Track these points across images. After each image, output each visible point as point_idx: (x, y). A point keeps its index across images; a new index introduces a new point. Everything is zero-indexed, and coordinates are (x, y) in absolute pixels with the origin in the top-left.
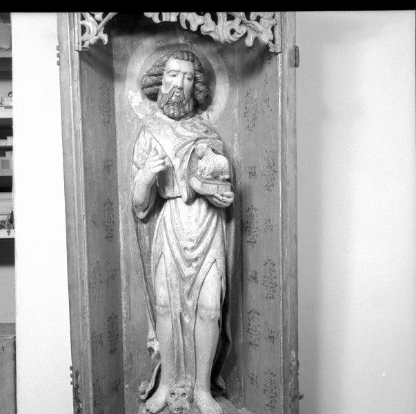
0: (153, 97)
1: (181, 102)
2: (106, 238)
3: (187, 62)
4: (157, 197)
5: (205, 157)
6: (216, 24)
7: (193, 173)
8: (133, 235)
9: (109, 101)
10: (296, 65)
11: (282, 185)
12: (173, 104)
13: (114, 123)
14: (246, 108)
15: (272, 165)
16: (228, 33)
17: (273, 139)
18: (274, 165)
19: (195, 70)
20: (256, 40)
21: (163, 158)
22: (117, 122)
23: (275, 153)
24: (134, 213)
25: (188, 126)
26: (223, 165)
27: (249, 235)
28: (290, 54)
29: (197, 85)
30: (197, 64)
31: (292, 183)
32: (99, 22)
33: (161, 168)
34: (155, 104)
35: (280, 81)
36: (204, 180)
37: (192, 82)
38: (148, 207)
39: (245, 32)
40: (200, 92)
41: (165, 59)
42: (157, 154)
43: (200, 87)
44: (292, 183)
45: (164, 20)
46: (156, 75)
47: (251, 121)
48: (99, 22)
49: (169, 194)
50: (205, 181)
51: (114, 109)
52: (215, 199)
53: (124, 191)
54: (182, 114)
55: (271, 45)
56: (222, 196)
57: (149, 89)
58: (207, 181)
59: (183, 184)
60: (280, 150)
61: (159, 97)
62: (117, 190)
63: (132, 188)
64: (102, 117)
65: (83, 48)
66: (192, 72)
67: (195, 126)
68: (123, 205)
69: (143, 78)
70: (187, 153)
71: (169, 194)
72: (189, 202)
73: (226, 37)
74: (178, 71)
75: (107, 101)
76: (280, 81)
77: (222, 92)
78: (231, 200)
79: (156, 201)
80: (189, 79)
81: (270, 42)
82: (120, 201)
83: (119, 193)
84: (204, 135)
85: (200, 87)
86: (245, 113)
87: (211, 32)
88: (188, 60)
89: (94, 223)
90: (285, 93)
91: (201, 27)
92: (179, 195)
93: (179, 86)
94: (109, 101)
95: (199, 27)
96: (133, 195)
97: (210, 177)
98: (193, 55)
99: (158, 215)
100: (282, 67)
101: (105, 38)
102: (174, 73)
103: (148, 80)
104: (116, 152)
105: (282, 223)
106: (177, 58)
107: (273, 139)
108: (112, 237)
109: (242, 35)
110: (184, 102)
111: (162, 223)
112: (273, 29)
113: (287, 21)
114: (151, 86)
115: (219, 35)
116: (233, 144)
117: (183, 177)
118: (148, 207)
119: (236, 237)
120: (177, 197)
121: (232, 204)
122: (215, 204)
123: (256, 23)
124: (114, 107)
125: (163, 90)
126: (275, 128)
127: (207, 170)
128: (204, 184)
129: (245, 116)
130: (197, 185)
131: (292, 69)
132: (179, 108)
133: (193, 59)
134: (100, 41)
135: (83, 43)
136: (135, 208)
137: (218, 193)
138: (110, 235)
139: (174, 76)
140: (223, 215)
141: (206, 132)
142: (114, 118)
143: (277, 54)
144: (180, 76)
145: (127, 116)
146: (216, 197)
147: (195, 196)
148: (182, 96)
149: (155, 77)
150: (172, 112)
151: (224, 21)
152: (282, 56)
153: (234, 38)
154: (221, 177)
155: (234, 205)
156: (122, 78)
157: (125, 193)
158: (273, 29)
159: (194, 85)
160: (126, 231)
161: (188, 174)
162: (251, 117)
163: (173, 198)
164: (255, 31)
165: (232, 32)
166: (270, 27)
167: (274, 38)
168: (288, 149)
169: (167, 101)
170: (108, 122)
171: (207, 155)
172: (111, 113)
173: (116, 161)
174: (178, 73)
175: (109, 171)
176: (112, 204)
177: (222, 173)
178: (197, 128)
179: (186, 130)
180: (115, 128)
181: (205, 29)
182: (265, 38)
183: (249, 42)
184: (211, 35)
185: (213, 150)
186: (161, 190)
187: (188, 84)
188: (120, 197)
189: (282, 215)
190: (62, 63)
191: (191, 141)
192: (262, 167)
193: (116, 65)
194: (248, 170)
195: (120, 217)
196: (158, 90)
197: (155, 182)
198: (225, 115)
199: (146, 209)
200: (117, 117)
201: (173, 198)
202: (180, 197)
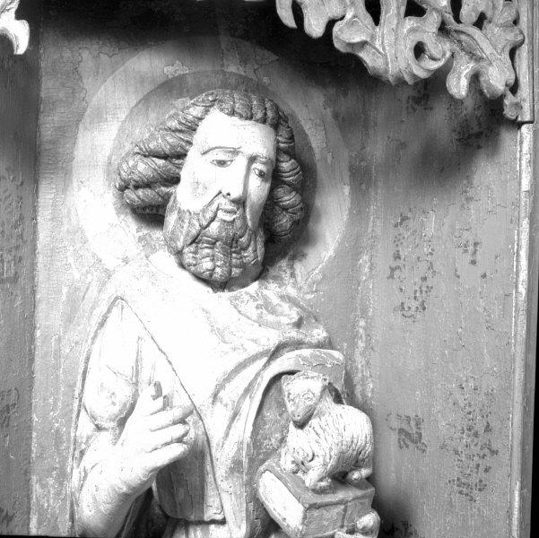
0: (152, 215)
5: (314, 422)
6: (377, 21)
7: (268, 455)
9: (21, 218)
12: (213, 244)
15: (480, 427)
16: (410, 54)
17: (487, 357)
18: (488, 429)
20: (475, 78)
22: (41, 276)
25: (251, 309)
26: (361, 442)
30: (284, 133)
37: (268, 185)
41: (196, 111)
42: (167, 404)
43: (288, 198)
46: (165, 157)
51: (34, 240)
53: (49, 472)
57: (140, 192)
61: (171, 219)
62: (27, 473)
63: (69, 471)
66: (272, 155)
67: (267, 306)
70: (247, 391)
73: (402, 65)
74: (235, 152)
80: (261, 174)
83: (34, 478)
84: (294, 334)
85: (288, 198)
86: (393, 270)
87: (363, 44)
91: (336, 29)
92: (219, 517)
94: (21, 218)
95: (331, 24)
96: (74, 504)
102: (222, 157)
103: (142, 167)
104: (32, 360)
106: (233, 113)
107: (487, 357)
110: (243, 240)
114: (148, 185)
117: (236, 466)
124: (35, 232)
127: (317, 463)
129: (391, 277)
132: (227, 254)
133: (278, 121)
139: (222, 163)
141: (298, 325)
142: (33, 266)
144: (241, 162)
145: (71, 260)
148: (238, 223)
149: (161, 162)
150: (206, 265)
156: (63, 168)
157: (51, 481)
161: (251, 460)
164: (472, 55)
165: (419, 50)
167: (517, 81)
169: (194, 232)
171: (321, 414)
172: (25, 251)
173: (31, 387)
174: (227, 153)
178: (273, 312)
179: (255, 318)
180: (34, 292)
184: (364, 55)
187: (257, 189)
188: (37, 489)
191: (262, 354)
193: (49, 124)
197: (150, 480)
200: (41, 259)
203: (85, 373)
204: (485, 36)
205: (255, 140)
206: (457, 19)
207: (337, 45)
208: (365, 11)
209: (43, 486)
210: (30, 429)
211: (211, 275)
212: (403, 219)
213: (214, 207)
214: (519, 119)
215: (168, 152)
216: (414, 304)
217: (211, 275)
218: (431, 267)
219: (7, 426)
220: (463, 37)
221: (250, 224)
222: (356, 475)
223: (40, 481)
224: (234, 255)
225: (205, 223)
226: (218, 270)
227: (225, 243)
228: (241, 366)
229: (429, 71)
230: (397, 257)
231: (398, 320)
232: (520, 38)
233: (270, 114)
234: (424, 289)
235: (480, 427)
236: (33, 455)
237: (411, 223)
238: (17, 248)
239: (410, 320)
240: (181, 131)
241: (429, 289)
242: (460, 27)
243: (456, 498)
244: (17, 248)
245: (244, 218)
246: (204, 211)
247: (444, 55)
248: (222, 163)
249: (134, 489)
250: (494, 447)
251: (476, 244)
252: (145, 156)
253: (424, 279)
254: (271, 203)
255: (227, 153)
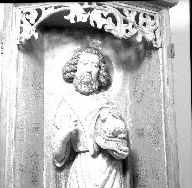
0: (70, 80)
1: (90, 82)
2: (32, 182)
3: (95, 55)
4: (71, 151)
6: (116, 25)
8: (52, 181)
10: (172, 57)
11: (166, 142)
13: (43, 98)
14: (135, 89)
15: (156, 127)
16: (125, 32)
18: (158, 127)
19: (100, 61)
20: (144, 38)
21: (76, 121)
23: (159, 119)
24: (54, 163)
26: (121, 127)
27: (140, 181)
28: (167, 48)
29: (101, 72)
31: (173, 141)
32: (32, 25)
33: (72, 129)
34: (71, 86)
35: (161, 67)
36: (107, 138)
37: (98, 68)
38: (64, 158)
39: (136, 32)
40: (104, 77)
44: (173, 141)
45: (78, 21)
46: (73, 65)
47: (139, 97)
48: (32, 25)
49: (80, 148)
50: (109, 139)
51: (44, 89)
52: (115, 153)
54: (91, 91)
55: (154, 42)
56: (120, 150)
58: (109, 139)
59: (91, 140)
60: (163, 116)
61: (75, 80)
62: (43, 145)
64: (34, 93)
65: (20, 42)
66: (99, 63)
68: (47, 156)
69: (64, 67)
71: (80, 148)
72: (95, 156)
73: (123, 34)
75: (39, 82)
76: (161, 67)
77: (118, 76)
78: (127, 154)
79: (71, 154)
80: (96, 67)
81: (153, 40)
82: (44, 153)
83: (44, 147)
86: (135, 92)
87: (111, 30)
88: (95, 54)
89: (22, 170)
90: (166, 75)
91: (105, 27)
92: (87, 150)
93: (89, 71)
94: (40, 83)
95: (104, 26)
97: (111, 135)
98: (99, 51)
99: (72, 164)
100: (163, 57)
101: (36, 35)
104: (43, 118)
105: (168, 173)
106: (87, 52)
108: (36, 181)
109: (134, 34)
110: (92, 82)
111: (74, 171)
112: (154, 32)
113: (165, 27)
115: (118, 32)
116: (126, 113)
117: (91, 136)
118: (64, 158)
119: (130, 182)
120: (86, 151)
121: (127, 158)
122: (115, 157)
123: (143, 27)
125: (78, 74)
126: (158, 101)
128: (106, 141)
129: (134, 94)
130: (103, 144)
131: (170, 59)
134: (33, 37)
135: (21, 38)
136: (56, 158)
137: (117, 148)
138: (35, 180)
139: (85, 64)
140: (121, 165)
141: (108, 104)
143: (158, 48)
146: (115, 152)
147: (101, 151)
148: (90, 78)
149: (72, 66)
151: (121, 23)
152: (162, 50)
153: (128, 35)
154: (119, 136)
155: (129, 157)
157: (49, 148)
158: (154, 32)
159: (99, 72)
160: (48, 177)
161: (94, 134)
162: (138, 95)
163: (84, 152)
164: (143, 32)
165: (127, 31)
166: (153, 31)
168: (169, 116)
169: (80, 81)
170: (39, 97)
172: (41, 91)
175: (37, 131)
176: (38, 156)
177: (120, 133)
180: (44, 101)
181: (107, 28)
182: (150, 37)
183: (139, 39)
184: (112, 32)
185: (114, 116)
186: (74, 146)
187: (95, 71)
188: (45, 150)
189: (167, 166)
190: (4, 53)
192: (148, 129)
194: (138, 132)
195: (44, 165)
196: (74, 75)
198: (121, 94)
199: (63, 160)
201: (84, 152)
202: (88, 151)
203: (66, 152)
204: (147, 28)
205: (95, 59)
206: (138, 24)
207: (106, 30)
208: (112, 23)
209: (47, 149)
210: (43, 134)
211: (84, 91)
212: (136, 79)
213: (84, 75)
214: (158, 47)
215: (73, 63)
216: (140, 99)
217: (84, 91)
218: (143, 89)
219: (37, 132)
220: (139, 28)
221: (94, 79)
222: (119, 136)
223: (46, 148)
224: (90, 87)
225: (82, 79)
226: (86, 90)
227: (87, 83)
228: (92, 112)
229: (131, 36)
230: (135, 89)
231: (137, 105)
232: (156, 28)
233: (97, 52)
234: (142, 95)
235: (156, 127)
236: (44, 142)
237: (138, 79)
238: (39, 90)
239: (139, 104)
240: (76, 58)
241: (143, 95)
242: (139, 26)
243: (152, 148)
244: (39, 90)
245: (92, 77)
246: (82, 76)
247: (134, 32)
248: (85, 64)
249: (65, 139)
250: (160, 132)
251: (152, 81)
252: (68, 65)
253: (142, 93)
254: (99, 74)
255: (89, 62)
